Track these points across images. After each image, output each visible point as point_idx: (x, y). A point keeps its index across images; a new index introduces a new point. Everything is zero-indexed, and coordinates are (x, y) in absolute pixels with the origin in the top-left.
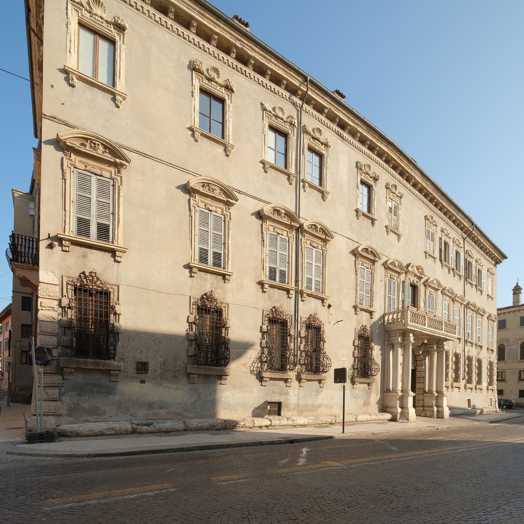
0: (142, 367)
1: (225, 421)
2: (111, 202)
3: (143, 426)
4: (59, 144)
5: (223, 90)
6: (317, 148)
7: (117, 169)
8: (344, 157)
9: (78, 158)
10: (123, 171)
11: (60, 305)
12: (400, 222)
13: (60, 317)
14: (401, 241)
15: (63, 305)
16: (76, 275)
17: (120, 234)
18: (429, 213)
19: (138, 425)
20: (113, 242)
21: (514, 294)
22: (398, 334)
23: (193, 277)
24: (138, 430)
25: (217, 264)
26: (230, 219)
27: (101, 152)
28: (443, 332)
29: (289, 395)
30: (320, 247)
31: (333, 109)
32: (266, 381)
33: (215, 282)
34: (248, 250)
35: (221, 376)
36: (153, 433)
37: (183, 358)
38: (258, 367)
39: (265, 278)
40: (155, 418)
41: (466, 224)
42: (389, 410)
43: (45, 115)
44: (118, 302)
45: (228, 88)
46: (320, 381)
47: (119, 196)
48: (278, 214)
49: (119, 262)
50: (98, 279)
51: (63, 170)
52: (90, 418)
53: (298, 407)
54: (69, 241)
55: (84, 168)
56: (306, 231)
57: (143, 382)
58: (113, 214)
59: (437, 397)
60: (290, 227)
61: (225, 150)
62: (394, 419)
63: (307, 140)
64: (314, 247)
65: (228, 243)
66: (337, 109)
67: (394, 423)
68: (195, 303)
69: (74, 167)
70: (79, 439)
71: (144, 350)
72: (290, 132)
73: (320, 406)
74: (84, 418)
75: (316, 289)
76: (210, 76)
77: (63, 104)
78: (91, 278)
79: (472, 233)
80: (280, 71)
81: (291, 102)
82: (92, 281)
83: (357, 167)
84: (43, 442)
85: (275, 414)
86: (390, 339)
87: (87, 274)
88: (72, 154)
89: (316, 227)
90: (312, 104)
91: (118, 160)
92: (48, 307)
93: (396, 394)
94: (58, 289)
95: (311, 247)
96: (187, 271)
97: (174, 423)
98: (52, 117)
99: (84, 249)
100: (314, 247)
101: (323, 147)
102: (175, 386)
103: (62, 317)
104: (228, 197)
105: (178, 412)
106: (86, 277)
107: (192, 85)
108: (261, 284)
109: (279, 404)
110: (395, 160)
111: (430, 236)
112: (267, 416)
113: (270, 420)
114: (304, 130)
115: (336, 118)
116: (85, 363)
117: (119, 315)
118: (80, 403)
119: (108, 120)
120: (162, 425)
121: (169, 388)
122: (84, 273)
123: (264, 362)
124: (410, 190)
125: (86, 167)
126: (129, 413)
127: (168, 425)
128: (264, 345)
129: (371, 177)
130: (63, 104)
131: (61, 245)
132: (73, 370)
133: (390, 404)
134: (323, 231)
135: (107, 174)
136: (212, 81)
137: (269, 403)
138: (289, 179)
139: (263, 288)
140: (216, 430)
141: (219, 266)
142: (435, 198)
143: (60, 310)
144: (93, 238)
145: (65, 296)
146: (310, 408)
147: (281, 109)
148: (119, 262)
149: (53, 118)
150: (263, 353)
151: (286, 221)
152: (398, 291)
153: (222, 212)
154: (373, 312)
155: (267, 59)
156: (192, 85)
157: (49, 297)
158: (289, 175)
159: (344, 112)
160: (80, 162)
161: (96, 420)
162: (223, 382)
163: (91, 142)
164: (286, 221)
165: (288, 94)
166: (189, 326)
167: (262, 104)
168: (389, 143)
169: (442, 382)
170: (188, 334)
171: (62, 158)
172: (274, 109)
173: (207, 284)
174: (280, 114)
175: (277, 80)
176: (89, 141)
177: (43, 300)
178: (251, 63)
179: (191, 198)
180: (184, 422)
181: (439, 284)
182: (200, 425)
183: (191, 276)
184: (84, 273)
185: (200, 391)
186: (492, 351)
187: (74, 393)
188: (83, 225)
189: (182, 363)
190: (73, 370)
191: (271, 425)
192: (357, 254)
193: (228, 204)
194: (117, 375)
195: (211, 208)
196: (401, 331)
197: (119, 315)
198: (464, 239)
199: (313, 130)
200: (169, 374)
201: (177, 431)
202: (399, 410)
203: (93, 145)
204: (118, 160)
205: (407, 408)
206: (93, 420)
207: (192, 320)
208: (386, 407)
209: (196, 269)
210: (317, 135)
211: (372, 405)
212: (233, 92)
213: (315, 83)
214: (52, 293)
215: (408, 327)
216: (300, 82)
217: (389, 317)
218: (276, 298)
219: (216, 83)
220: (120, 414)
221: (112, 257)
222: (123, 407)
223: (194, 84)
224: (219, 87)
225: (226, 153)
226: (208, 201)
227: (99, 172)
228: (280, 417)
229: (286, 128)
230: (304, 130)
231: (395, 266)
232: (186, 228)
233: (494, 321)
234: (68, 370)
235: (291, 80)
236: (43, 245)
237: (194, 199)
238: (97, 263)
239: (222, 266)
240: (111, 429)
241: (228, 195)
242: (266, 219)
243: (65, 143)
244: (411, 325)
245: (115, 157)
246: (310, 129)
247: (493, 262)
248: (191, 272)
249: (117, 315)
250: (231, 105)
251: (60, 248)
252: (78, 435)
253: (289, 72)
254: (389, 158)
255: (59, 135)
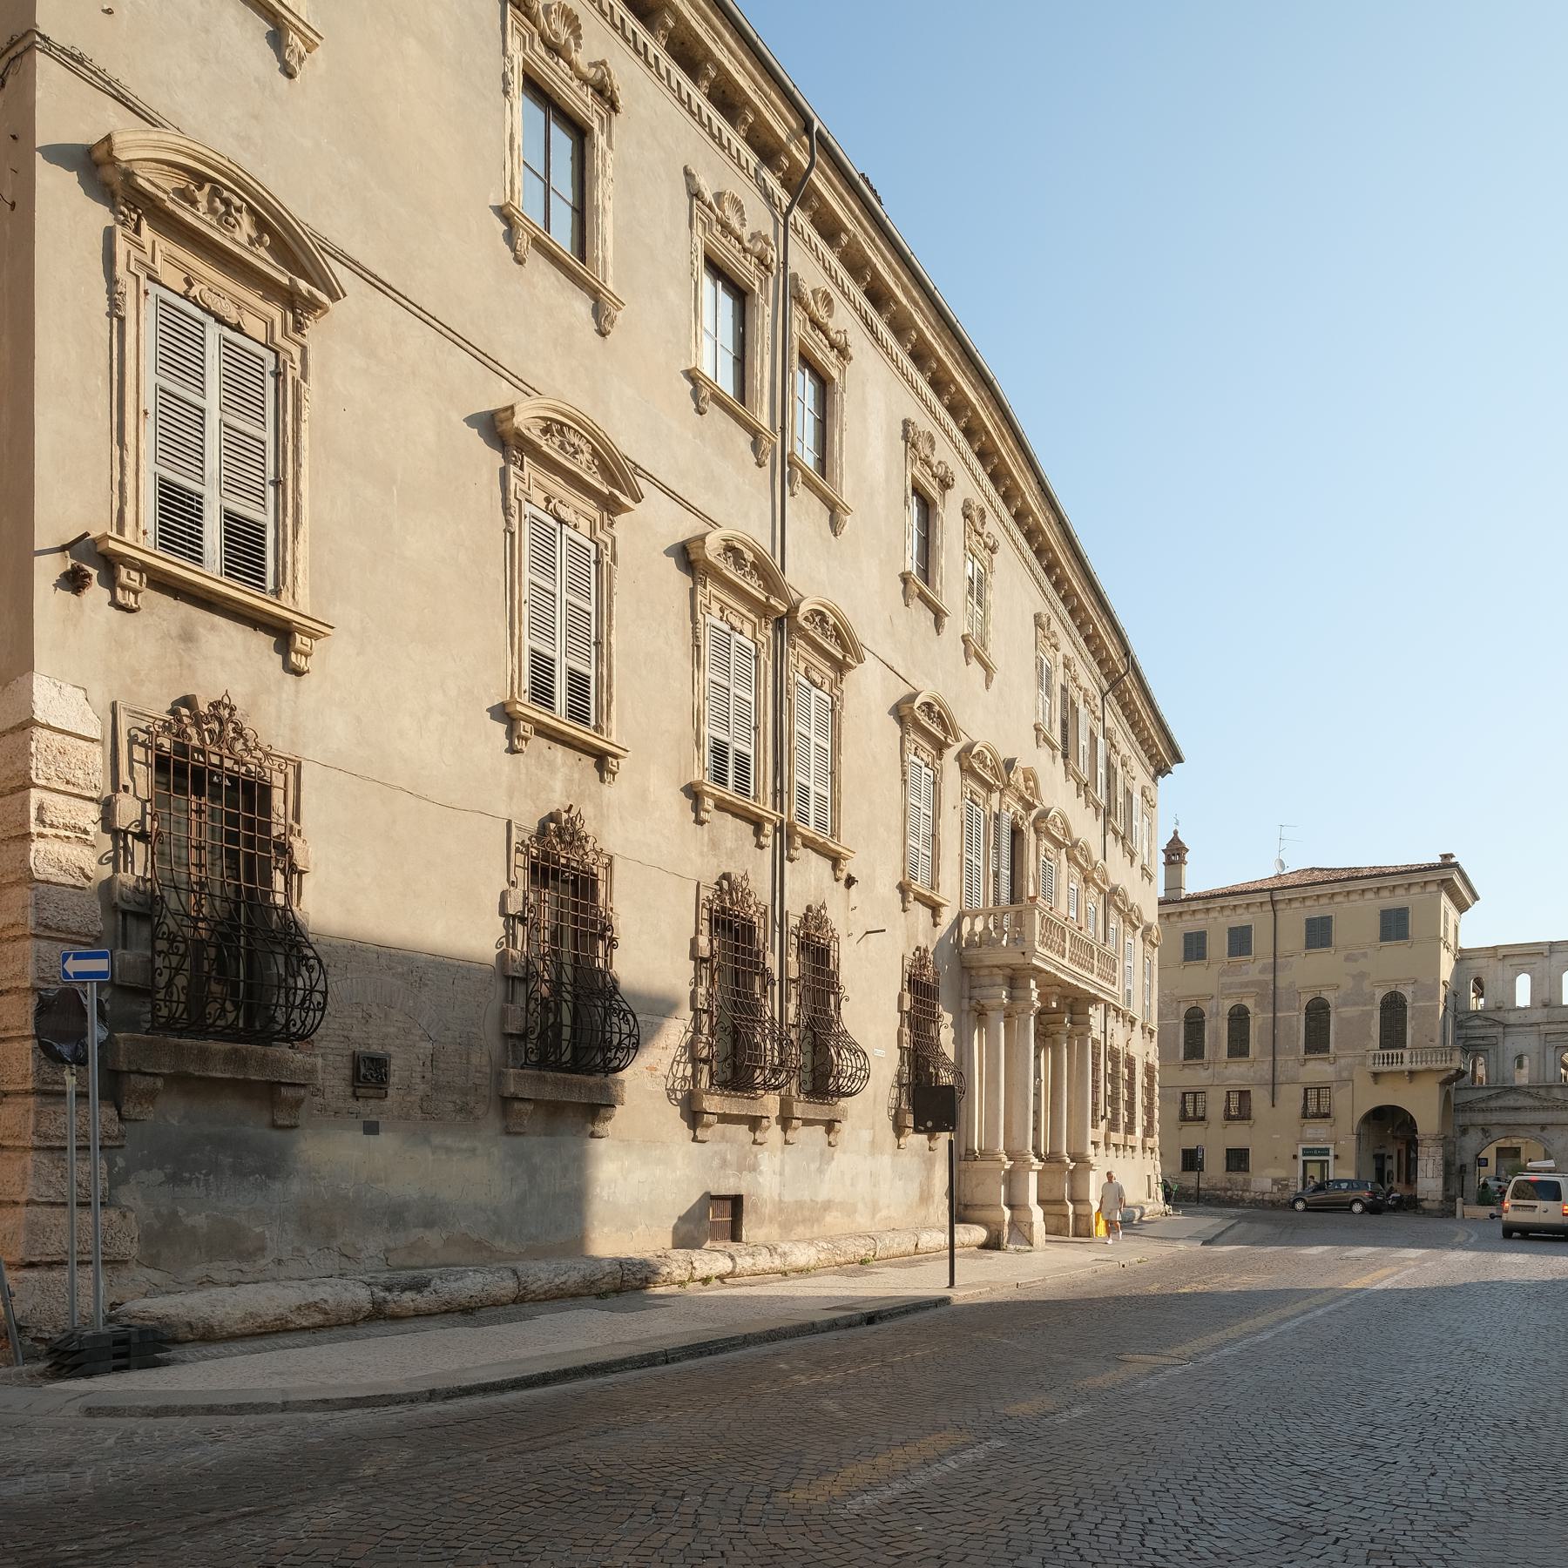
0: (369, 1074)
1: (621, 1263)
2: (269, 436)
3: (403, 1291)
4: (96, 168)
5: (587, 94)
6: (819, 356)
7: (290, 316)
8: (880, 396)
9: (164, 245)
10: (312, 326)
11: (107, 822)
12: (990, 628)
13: (108, 870)
14: (994, 685)
15: (121, 822)
16: (161, 709)
17: (300, 566)
18: (1045, 610)
19: (389, 1289)
20: (277, 592)
21: (1169, 863)
22: (1000, 980)
23: (520, 752)
24: (391, 1308)
25: (578, 714)
26: (614, 558)
27: (244, 240)
28: (1094, 977)
29: (761, 1173)
30: (826, 687)
31: (861, 238)
32: (708, 1126)
33: (576, 776)
34: (664, 681)
35: (597, 1108)
36: (430, 1314)
37: (490, 1041)
38: (684, 1078)
39: (700, 773)
40: (414, 1261)
41: (1114, 651)
42: (978, 1214)
43: (43, 37)
44: (296, 826)
45: (604, 93)
46: (830, 1126)
47: (297, 418)
48: (735, 563)
49: (298, 673)
50: (239, 732)
51: (112, 280)
52: (219, 1271)
53: (781, 1210)
54: (140, 571)
55: (182, 288)
56: (801, 628)
57: (371, 1129)
58: (278, 483)
59: (1009, 1172)
60: (763, 610)
61: (598, 311)
62: (993, 1244)
63: (799, 327)
64: (813, 683)
65: (609, 644)
66: (873, 241)
67: (996, 1254)
68: (524, 848)
69: (150, 278)
70: (213, 1349)
71: (375, 1010)
72: (757, 289)
73: (827, 1206)
74: (197, 1271)
75: (820, 824)
76: (556, 34)
77: (109, 12)
78: (215, 726)
79: (1123, 681)
80: (744, 78)
81: (757, 185)
82: (218, 738)
83: (905, 437)
84: (126, 1368)
85: (723, 1238)
86: (976, 992)
87: (204, 708)
88: (144, 223)
89: (824, 620)
90: (811, 207)
91: (303, 285)
92: (66, 827)
93: (998, 1165)
94: (98, 757)
95: (806, 683)
96: (500, 729)
97: (489, 1277)
98: (72, 56)
99: (185, 609)
100: (813, 683)
101: (833, 355)
102: (465, 1145)
103: (116, 869)
104: (612, 483)
105: (475, 1237)
106: (198, 720)
107: (504, 52)
108: (693, 793)
109: (736, 1202)
110: (988, 433)
111: (1044, 677)
112: (708, 1244)
113: (732, 1258)
114: (794, 292)
115: (864, 267)
116: (203, 1056)
117: (301, 873)
118: (181, 1211)
119: (256, 117)
120: (454, 1285)
121: (448, 1150)
122: (188, 701)
123: (701, 1060)
124: (1007, 530)
125: (191, 285)
126: (334, 1244)
127: (472, 1284)
128: (702, 1003)
129: (934, 476)
130: (109, 12)
131: (110, 581)
132: (160, 1083)
133: (979, 1196)
134: (839, 636)
135: (255, 327)
136: (559, 54)
137: (713, 1198)
138: (755, 446)
139: (697, 807)
140: (599, 1296)
141: (584, 720)
142: (1058, 563)
143: (107, 842)
144: (210, 571)
145: (126, 788)
146: (807, 1213)
147: (739, 207)
148: (298, 673)
149: (74, 61)
150: (697, 1030)
151: (753, 586)
152: (987, 843)
153: (593, 530)
154: (941, 905)
155: (713, 28)
156: (504, 52)
157: (70, 788)
158: (755, 433)
159: (889, 256)
160: (170, 260)
161: (235, 1277)
162: (600, 1128)
163: (215, 193)
164: (753, 586)
165: (753, 160)
166: (506, 927)
167: (687, 173)
168: (984, 381)
169: (1085, 1127)
170: (502, 956)
171: (109, 235)
172: (719, 196)
173: (555, 780)
174: (735, 223)
175: (727, 101)
176: (207, 187)
177: (47, 797)
178: (664, 26)
179: (513, 469)
180: (515, 1272)
181: (1067, 831)
182: (557, 1281)
183: (512, 750)
184: (188, 701)
185: (537, 1160)
186: (1151, 1033)
187: (157, 1175)
188: (178, 507)
189: (485, 1060)
190: (160, 1083)
191: (732, 1274)
192: (908, 719)
193: (611, 507)
194: (298, 1103)
195: (565, 513)
196: (1008, 972)
197: (301, 873)
198: (1104, 695)
199: (814, 292)
200: (447, 1107)
201: (497, 1303)
202: (1007, 1213)
203: (222, 209)
204: (303, 285)
205: (1026, 1207)
206: (225, 1276)
207: (514, 907)
208: (966, 1206)
209: (528, 727)
210: (821, 313)
211: (937, 1199)
212: (616, 111)
213: (829, 145)
214: (79, 773)
215: (1034, 961)
216: (790, 128)
217: (972, 924)
218: (729, 844)
219: (570, 63)
220: (308, 1251)
221: (278, 649)
222: (320, 1224)
223: (510, 52)
224: (575, 83)
225: (598, 323)
226: (556, 486)
227: (232, 315)
228: (733, 1247)
229: (746, 270)
230: (794, 292)
231: (985, 766)
232: (496, 573)
233: (1154, 945)
234: (144, 1083)
235: (768, 116)
236: (47, 570)
237: (517, 470)
238: (229, 663)
239: (593, 723)
240: (308, 1306)
241: (612, 475)
242: (706, 574)
243: (129, 175)
244: (1045, 958)
245: (293, 273)
246: (807, 290)
247: (1152, 770)
248: (510, 733)
249: (295, 877)
250: (610, 155)
251: (105, 594)
252: (208, 1336)
253: (765, 87)
254: (975, 424)
255: (117, 139)
